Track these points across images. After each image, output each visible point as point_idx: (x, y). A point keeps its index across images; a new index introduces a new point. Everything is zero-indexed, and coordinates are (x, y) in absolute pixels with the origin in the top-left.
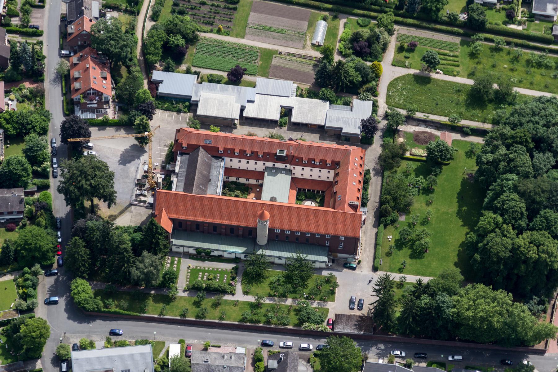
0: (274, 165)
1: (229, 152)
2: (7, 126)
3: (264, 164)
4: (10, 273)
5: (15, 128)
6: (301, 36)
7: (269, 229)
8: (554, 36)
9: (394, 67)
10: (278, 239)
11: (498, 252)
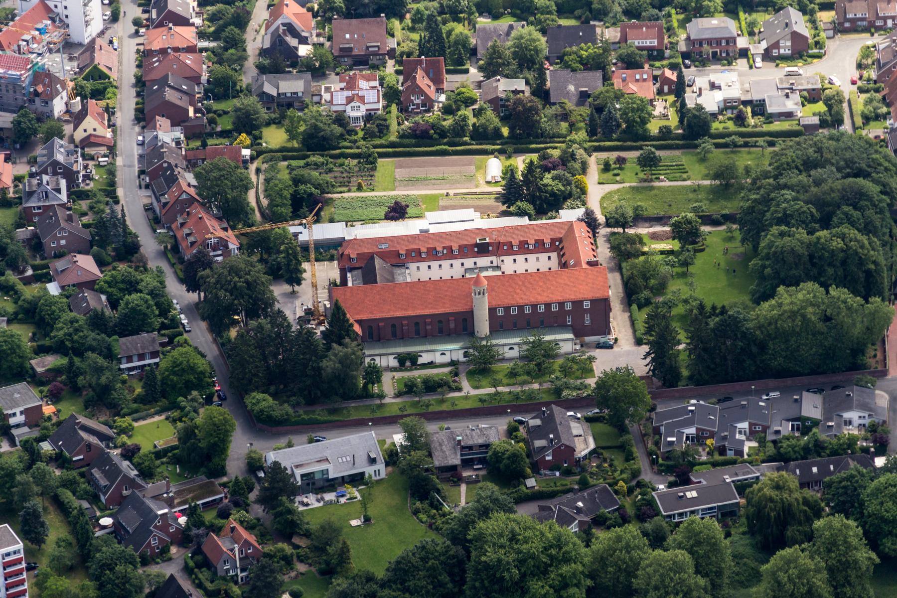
0: (475, 263)
1: (413, 254)
2: (110, 290)
3: (462, 264)
4: (158, 413)
6: (471, 178)
8: (803, 126)
9: (602, 186)
10: (503, 323)
11: (792, 249)
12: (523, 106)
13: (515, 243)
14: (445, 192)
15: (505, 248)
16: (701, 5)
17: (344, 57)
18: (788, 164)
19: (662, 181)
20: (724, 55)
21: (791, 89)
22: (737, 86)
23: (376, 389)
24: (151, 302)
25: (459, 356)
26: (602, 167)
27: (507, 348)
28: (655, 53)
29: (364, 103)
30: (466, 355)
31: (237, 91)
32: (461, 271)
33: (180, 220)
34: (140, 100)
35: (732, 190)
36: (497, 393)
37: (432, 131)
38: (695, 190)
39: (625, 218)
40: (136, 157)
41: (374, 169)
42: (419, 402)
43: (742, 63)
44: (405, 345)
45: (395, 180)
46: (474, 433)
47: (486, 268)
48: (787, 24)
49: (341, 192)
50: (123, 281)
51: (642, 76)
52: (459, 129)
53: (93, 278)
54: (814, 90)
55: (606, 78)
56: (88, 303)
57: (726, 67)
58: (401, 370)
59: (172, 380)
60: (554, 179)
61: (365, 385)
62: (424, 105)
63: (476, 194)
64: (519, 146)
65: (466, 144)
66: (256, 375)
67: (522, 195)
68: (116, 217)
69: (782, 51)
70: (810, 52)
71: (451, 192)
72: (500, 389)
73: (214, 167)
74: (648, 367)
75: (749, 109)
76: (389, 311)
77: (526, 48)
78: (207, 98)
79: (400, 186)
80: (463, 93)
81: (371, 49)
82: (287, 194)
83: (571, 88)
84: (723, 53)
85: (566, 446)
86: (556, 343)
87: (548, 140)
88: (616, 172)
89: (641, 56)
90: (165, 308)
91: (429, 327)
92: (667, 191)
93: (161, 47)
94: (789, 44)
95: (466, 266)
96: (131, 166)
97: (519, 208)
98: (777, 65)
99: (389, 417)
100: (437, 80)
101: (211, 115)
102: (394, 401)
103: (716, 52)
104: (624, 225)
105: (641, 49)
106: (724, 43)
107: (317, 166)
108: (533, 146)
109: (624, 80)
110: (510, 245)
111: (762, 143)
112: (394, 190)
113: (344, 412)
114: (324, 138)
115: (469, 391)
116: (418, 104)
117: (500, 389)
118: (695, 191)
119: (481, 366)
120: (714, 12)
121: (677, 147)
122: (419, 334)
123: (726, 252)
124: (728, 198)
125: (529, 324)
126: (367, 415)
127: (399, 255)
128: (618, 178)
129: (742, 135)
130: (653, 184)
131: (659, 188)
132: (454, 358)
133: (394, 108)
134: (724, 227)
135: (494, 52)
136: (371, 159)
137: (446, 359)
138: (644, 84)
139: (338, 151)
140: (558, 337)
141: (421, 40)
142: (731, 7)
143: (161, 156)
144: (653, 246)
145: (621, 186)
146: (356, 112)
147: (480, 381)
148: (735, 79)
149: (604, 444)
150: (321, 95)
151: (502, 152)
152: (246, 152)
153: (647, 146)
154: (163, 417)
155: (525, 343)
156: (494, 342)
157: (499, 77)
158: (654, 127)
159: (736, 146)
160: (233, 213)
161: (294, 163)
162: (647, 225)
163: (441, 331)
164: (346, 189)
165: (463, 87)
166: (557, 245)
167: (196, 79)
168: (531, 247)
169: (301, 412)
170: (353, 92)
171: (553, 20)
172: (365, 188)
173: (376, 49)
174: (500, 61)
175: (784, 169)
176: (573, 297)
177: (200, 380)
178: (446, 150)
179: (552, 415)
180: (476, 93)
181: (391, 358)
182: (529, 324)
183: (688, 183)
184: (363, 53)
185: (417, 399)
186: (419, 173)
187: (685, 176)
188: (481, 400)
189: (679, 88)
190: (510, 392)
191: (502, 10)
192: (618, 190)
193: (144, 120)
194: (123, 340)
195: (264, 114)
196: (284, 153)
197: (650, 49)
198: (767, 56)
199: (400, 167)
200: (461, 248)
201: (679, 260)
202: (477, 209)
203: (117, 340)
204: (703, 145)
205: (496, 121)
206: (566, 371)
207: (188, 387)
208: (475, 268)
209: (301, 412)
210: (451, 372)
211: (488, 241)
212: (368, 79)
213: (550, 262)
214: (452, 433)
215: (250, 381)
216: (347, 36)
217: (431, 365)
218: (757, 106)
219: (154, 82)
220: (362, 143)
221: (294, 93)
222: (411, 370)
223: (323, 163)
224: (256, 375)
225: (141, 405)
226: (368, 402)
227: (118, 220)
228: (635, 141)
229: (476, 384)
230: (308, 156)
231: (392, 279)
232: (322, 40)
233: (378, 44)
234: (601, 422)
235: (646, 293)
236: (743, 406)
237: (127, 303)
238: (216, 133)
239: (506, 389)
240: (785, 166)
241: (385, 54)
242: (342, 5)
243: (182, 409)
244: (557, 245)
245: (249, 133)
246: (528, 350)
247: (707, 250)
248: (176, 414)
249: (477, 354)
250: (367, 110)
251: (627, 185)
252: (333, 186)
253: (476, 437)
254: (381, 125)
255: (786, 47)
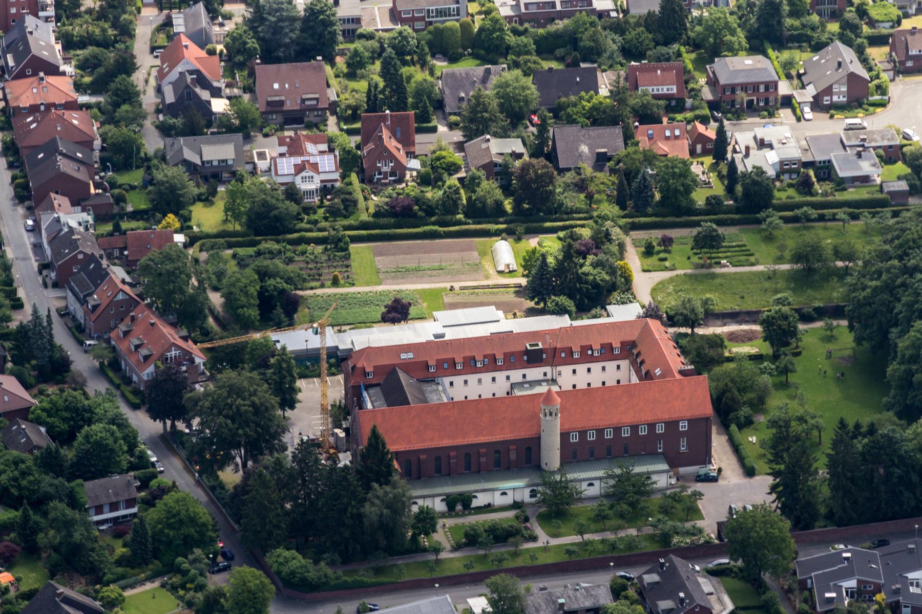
0: (524, 376)
1: (446, 366)
3: (508, 378)
4: (150, 579)
5: (64, 420)
6: (477, 268)
7: (561, 434)
8: (889, 193)
9: (647, 274)
10: (577, 452)
12: (536, 172)
13: (576, 349)
14: (448, 285)
15: (563, 355)
16: (722, 41)
17: (272, 113)
18: (914, 241)
19: (725, 266)
20: (762, 104)
21: (863, 146)
22: (792, 143)
23: (424, 541)
24: (118, 434)
25: (525, 496)
26: (643, 249)
27: (584, 485)
28: (673, 103)
29: (318, 173)
30: (533, 494)
31: (141, 158)
32: (506, 386)
33: (123, 327)
34: (17, 172)
35: (817, 277)
36: (586, 544)
37: (416, 208)
38: (770, 276)
39: (696, 314)
40: (29, 247)
41: (348, 257)
42: (485, 556)
43: (785, 114)
44: (454, 484)
45: (378, 271)
46: (578, 594)
47: (538, 382)
48: (840, 64)
49: (312, 288)
50: (67, 409)
51: (673, 132)
52: (449, 205)
53: (25, 405)
54: (891, 147)
55: (628, 137)
56: (28, 437)
57: (767, 120)
58: (450, 516)
59: (168, 536)
60: (595, 265)
61: (414, 536)
62: (393, 174)
63: (488, 287)
64: (530, 225)
65: (459, 223)
66: (277, 527)
67: (547, 286)
68: (40, 325)
69: (835, 98)
70: (870, 98)
71: (457, 285)
72: (587, 537)
73: (165, 257)
74: (775, 504)
75: (812, 173)
76: (432, 440)
77: (513, 97)
78: (105, 169)
79: (386, 278)
80: (444, 157)
81: (307, 103)
82: (253, 290)
83: (584, 149)
84: (763, 102)
85: (701, 607)
86: (648, 476)
87: (565, 217)
88: (662, 255)
89: (658, 106)
90: (131, 441)
91: (483, 460)
92: (735, 279)
93: (32, 103)
94: (844, 89)
95: (513, 380)
96: (25, 259)
97: (557, 304)
98: (832, 117)
99: (455, 576)
100: (407, 142)
101: (116, 191)
102: (452, 555)
103: (753, 100)
104: (693, 324)
105: (657, 97)
106: (762, 89)
107: (272, 254)
108: (548, 224)
109: (651, 138)
110: (570, 352)
111: (843, 216)
112: (380, 284)
113: (395, 570)
114: (278, 219)
115: (545, 541)
116: (386, 173)
117: (587, 537)
118: (769, 278)
119: (556, 507)
120: (738, 50)
121: (733, 223)
122: (469, 469)
123: (829, 355)
124: (813, 286)
125: (592, 454)
126: (423, 575)
127: (427, 367)
128: (667, 264)
129: (815, 206)
130: (713, 270)
131: (723, 275)
132: (518, 499)
133: (354, 177)
134: (819, 324)
135: (478, 104)
136: (342, 244)
137: (508, 500)
138: (677, 142)
139: (296, 235)
140: (652, 468)
141: (369, 90)
142: (756, 42)
143: (74, 245)
144: (734, 350)
145: (674, 273)
146: (309, 185)
147: (559, 527)
148: (789, 135)
149: (741, 605)
150: (254, 163)
151: (510, 233)
152: (179, 238)
153: (706, 221)
154: (157, 584)
155: (610, 477)
156: (570, 476)
157: (488, 137)
158: (699, 197)
159: (809, 220)
160: (188, 315)
161: (241, 251)
162: (719, 323)
163: (498, 464)
164: (317, 284)
165: (441, 149)
166: (629, 350)
167: (87, 144)
168: (596, 354)
169: (340, 572)
170: (303, 158)
171: (535, 62)
172: (342, 282)
173: (314, 102)
174: (486, 115)
175: (910, 248)
176: (666, 416)
177: (202, 534)
178: (436, 231)
179: (673, 568)
180: (458, 157)
181: (438, 500)
182: (592, 454)
183: (760, 268)
184: (298, 108)
185: (482, 552)
186: (410, 261)
187: (752, 259)
188: (569, 552)
189: (718, 148)
190: (603, 541)
191: (460, 50)
192: (671, 280)
193: (29, 198)
194: (89, 485)
195: (193, 189)
196: (224, 238)
197: (668, 97)
198: (817, 105)
199: (380, 254)
200: (507, 356)
201: (778, 367)
202: (499, 306)
203: (83, 485)
204: (769, 220)
205: (498, 194)
206: (665, 510)
207: (188, 544)
208: (525, 383)
209: (340, 572)
210: (517, 517)
211: (541, 346)
212: (315, 141)
213: (604, 374)
214: (550, 594)
215: (270, 533)
216: (276, 86)
217: (488, 508)
218: (821, 168)
219: (36, 149)
220: (324, 224)
221: (223, 161)
222: (463, 515)
223: (280, 252)
224: (277, 527)
225: (128, 569)
226: (420, 558)
227: (44, 328)
228: (678, 217)
229: (554, 530)
230: (259, 242)
231: (425, 400)
232: (236, 91)
233: (317, 96)
234: (728, 575)
235: (745, 411)
236: (911, 551)
237: (87, 437)
238: (126, 214)
239: (596, 537)
240: (911, 243)
241: (326, 109)
242: (257, 46)
243: (185, 573)
244: (629, 350)
245: (176, 214)
246: (614, 486)
247: (804, 353)
248: (176, 579)
249: (548, 491)
250: (322, 181)
251: (680, 272)
252: (304, 280)
253: (582, 599)
254: (347, 200)
255: (840, 95)
